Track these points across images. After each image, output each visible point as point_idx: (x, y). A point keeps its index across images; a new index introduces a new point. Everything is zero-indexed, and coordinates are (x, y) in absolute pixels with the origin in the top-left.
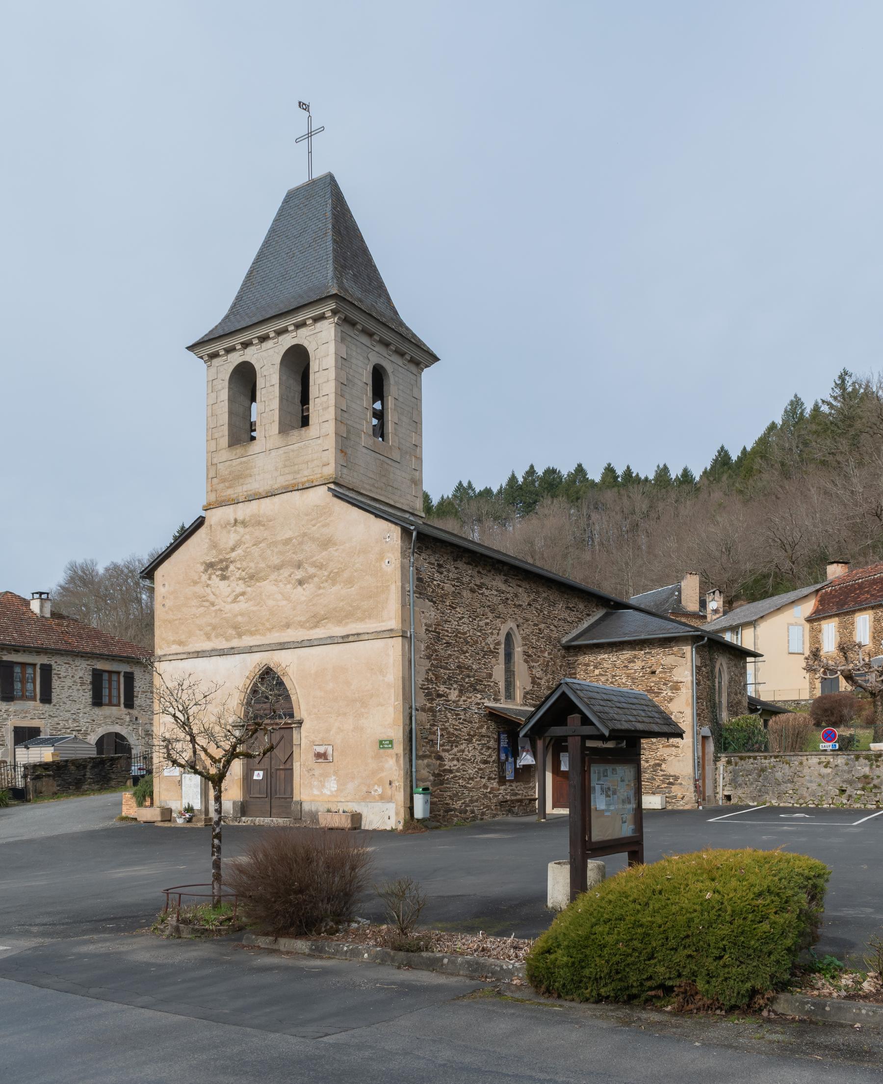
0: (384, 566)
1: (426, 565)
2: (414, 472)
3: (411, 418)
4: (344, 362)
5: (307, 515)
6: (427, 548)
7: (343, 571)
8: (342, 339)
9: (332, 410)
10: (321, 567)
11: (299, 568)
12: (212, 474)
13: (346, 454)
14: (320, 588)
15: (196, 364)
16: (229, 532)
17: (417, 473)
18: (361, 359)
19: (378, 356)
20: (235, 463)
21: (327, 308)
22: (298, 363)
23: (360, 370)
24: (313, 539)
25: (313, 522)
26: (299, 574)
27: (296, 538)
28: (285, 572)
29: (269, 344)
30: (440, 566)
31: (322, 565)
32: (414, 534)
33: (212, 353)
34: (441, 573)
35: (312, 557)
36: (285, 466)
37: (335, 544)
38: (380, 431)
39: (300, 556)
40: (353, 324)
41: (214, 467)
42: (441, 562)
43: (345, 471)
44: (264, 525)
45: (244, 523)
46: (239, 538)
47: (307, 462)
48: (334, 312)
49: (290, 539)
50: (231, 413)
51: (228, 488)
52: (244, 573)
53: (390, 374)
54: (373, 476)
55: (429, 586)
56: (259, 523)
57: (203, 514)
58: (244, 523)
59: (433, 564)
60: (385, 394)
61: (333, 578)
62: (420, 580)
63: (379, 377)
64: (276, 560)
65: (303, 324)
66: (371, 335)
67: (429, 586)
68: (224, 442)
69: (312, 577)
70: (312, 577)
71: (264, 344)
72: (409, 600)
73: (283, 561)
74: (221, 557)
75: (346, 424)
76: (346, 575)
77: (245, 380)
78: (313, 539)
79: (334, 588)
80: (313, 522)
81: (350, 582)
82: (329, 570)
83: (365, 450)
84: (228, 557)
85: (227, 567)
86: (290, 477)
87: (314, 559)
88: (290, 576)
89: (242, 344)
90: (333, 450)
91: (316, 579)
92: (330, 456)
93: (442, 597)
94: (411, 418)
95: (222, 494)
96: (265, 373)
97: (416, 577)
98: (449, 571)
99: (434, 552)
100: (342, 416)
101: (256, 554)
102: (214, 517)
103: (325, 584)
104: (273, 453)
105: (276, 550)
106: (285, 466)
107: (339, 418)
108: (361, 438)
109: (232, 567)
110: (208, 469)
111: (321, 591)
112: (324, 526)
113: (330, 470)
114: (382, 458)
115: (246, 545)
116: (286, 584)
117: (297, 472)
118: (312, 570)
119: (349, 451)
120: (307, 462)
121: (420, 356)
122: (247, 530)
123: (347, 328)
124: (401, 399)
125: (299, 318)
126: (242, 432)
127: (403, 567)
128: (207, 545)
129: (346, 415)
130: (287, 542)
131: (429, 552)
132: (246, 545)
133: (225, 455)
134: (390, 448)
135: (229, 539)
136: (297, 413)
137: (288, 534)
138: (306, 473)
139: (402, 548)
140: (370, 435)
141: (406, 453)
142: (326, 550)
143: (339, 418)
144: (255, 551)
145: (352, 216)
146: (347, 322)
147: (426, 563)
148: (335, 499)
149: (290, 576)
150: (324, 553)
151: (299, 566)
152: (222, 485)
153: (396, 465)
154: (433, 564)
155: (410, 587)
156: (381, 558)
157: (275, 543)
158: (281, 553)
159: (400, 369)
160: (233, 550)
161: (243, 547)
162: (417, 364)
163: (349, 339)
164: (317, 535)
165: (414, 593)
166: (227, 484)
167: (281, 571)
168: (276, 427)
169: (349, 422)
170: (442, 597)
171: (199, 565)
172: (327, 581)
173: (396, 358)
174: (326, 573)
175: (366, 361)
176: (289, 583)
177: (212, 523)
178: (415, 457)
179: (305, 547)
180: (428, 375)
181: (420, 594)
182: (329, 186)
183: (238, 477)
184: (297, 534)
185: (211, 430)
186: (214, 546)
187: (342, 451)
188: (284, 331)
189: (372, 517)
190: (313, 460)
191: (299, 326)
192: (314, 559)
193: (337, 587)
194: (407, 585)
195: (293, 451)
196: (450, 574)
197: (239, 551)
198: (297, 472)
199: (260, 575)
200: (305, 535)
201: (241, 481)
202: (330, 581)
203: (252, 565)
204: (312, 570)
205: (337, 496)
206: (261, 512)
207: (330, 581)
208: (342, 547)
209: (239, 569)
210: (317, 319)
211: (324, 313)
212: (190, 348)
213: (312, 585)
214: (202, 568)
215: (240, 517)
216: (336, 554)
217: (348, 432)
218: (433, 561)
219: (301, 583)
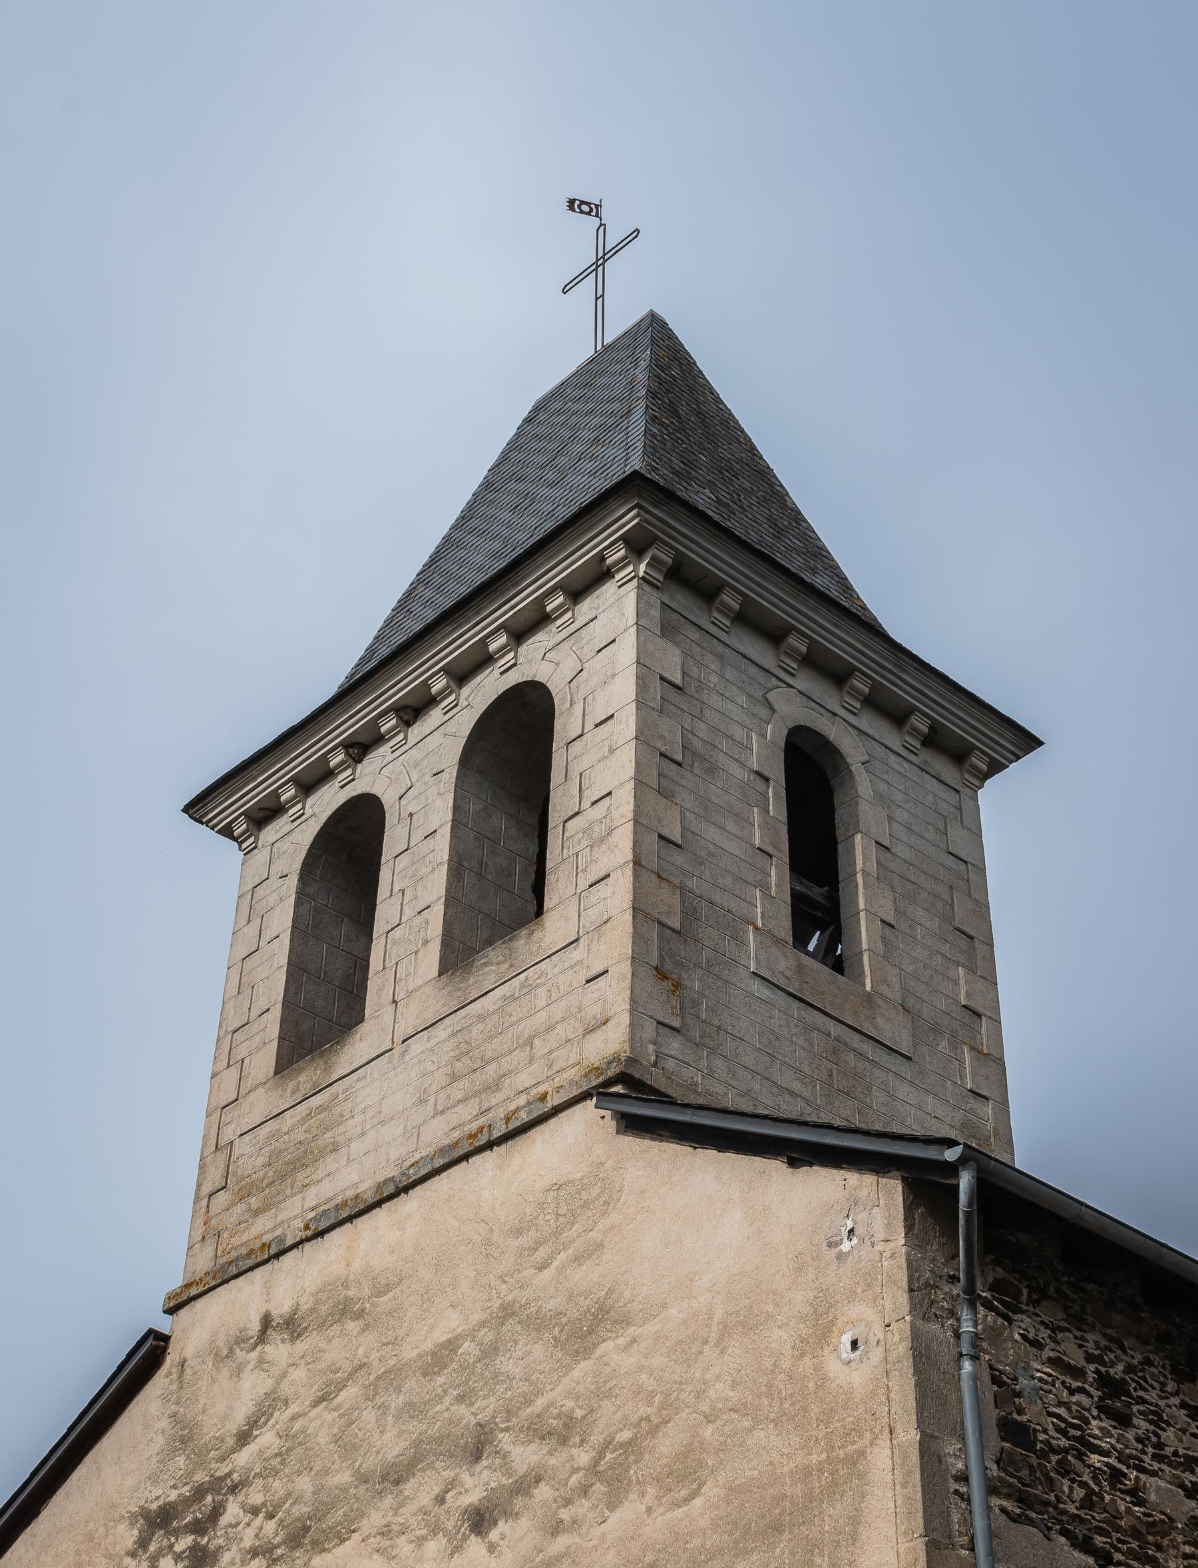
0: (833, 1367)
1: (1041, 1370)
2: (972, 1102)
3: (948, 918)
4: (671, 694)
5: (518, 1232)
6: (1040, 1296)
7: (654, 1431)
8: (663, 626)
9: (623, 839)
10: (562, 1432)
11: (477, 1458)
12: (214, 1179)
13: (677, 985)
14: (557, 1528)
15: (216, 860)
16: (238, 1373)
17: (988, 1110)
18: (742, 699)
19: (799, 702)
20: (289, 1120)
21: (605, 540)
22: (516, 749)
23: (739, 733)
24: (536, 1323)
25: (541, 1254)
26: (475, 1486)
27: (471, 1335)
28: (422, 1489)
29: (435, 716)
30: (1111, 1387)
31: (569, 1422)
32: (965, 1181)
33: (260, 807)
34: (1124, 1421)
35: (528, 1401)
36: (454, 1078)
37: (626, 1322)
38: (818, 913)
39: (487, 1407)
40: (707, 591)
41: (222, 1157)
42: (1117, 1371)
43: (674, 1045)
44: (360, 1315)
45: (293, 1326)
46: (269, 1384)
47: (530, 1041)
48: (636, 545)
49: (452, 1345)
50: (297, 968)
51: (256, 1213)
52: (271, 1526)
53: (856, 768)
54: (796, 1086)
55: (1065, 1470)
56: (346, 1310)
57: (164, 1324)
58: (293, 1326)
59: (1078, 1373)
60: (840, 834)
61: (611, 1478)
62: (1014, 1432)
63: (811, 775)
64: (391, 1445)
65: (538, 620)
66: (775, 636)
67: (1065, 1470)
68: (264, 1060)
69: (523, 1487)
70: (523, 1487)
71: (415, 732)
72: (968, 1521)
73: (417, 1444)
74: (201, 1477)
75: (682, 887)
76: (667, 1445)
77: (350, 853)
78: (536, 1323)
79: (614, 1518)
80: (541, 1254)
81: (685, 1475)
82: (597, 1438)
83: (757, 987)
84: (223, 1470)
85: (216, 1513)
86: (465, 1112)
87: (540, 1403)
88: (441, 1500)
89: (347, 745)
90: (626, 968)
91: (543, 1492)
92: (615, 995)
93: (1136, 1534)
94: (948, 918)
95: (236, 1241)
96: (411, 809)
97: (993, 1414)
98: (1158, 1419)
99: (1078, 1322)
100: (660, 857)
101: (323, 1438)
102: (193, 1333)
103: (583, 1507)
104: (416, 1045)
105: (395, 1401)
106: (454, 1078)
107: (652, 862)
108: (743, 943)
109: (233, 1511)
110: (202, 1168)
111: (561, 1542)
112: (579, 1259)
113: (610, 1043)
114: (833, 1028)
115: (294, 1408)
116: (420, 1541)
117: (495, 1086)
118: (525, 1456)
119: (694, 981)
120: (530, 1041)
121: (972, 738)
122: (300, 1346)
123: (682, 600)
124: (900, 850)
125: (521, 599)
126: (322, 1007)
127: (922, 1356)
128: (160, 1440)
129: (679, 858)
130: (439, 1358)
131: (1051, 1313)
132: (294, 1408)
133: (260, 1103)
134: (869, 998)
135: (225, 1401)
136: (502, 891)
137: (446, 1324)
138: (523, 1080)
139: (913, 1268)
140: (779, 942)
141: (936, 1030)
142: (585, 1352)
143: (653, 863)
144: (322, 1424)
145: (718, 400)
146: (678, 576)
147: (1048, 1368)
148: (632, 1144)
149: (441, 1500)
150: (582, 1369)
151: (478, 1447)
152: (240, 1208)
153: (895, 1063)
154: (1078, 1373)
155: (971, 1454)
156: (820, 1330)
157: (392, 1378)
158: (413, 1410)
159: (893, 759)
160: (244, 1438)
161: (281, 1417)
162: (959, 755)
163: (694, 635)
164: (554, 1303)
165: (992, 1489)
166: (254, 1202)
167: (409, 1488)
168: (431, 957)
169: (692, 883)
170: (1136, 1534)
171: (122, 1528)
172: (585, 1490)
173: (868, 722)
174: (584, 1457)
175: (764, 712)
176: (435, 1530)
177: (189, 1352)
178: (977, 1051)
179: (507, 1364)
180: (1002, 802)
181: (1023, 1500)
182: (656, 335)
183: (293, 1166)
184: (477, 1317)
185: (231, 1034)
186: (184, 1438)
187: (661, 974)
188: (481, 660)
189: (776, 1167)
190: (550, 1029)
191: (520, 633)
192: (540, 1403)
193: (630, 1510)
194: (951, 1447)
195: (482, 1018)
196: (1169, 1435)
197: (266, 1439)
198: (495, 1086)
199: (329, 1522)
200: (508, 1311)
201: (301, 1176)
202: (599, 1488)
203: (304, 1484)
204: (525, 1456)
205: (632, 1125)
206: (357, 1266)
207: (599, 1488)
208: (652, 1327)
209: (255, 1511)
210: (578, 590)
211: (601, 558)
212: (196, 808)
213: (524, 1523)
214: (128, 1536)
215: (281, 1307)
216: (628, 1361)
217: (690, 913)
218: (1076, 1358)
219: (480, 1521)
